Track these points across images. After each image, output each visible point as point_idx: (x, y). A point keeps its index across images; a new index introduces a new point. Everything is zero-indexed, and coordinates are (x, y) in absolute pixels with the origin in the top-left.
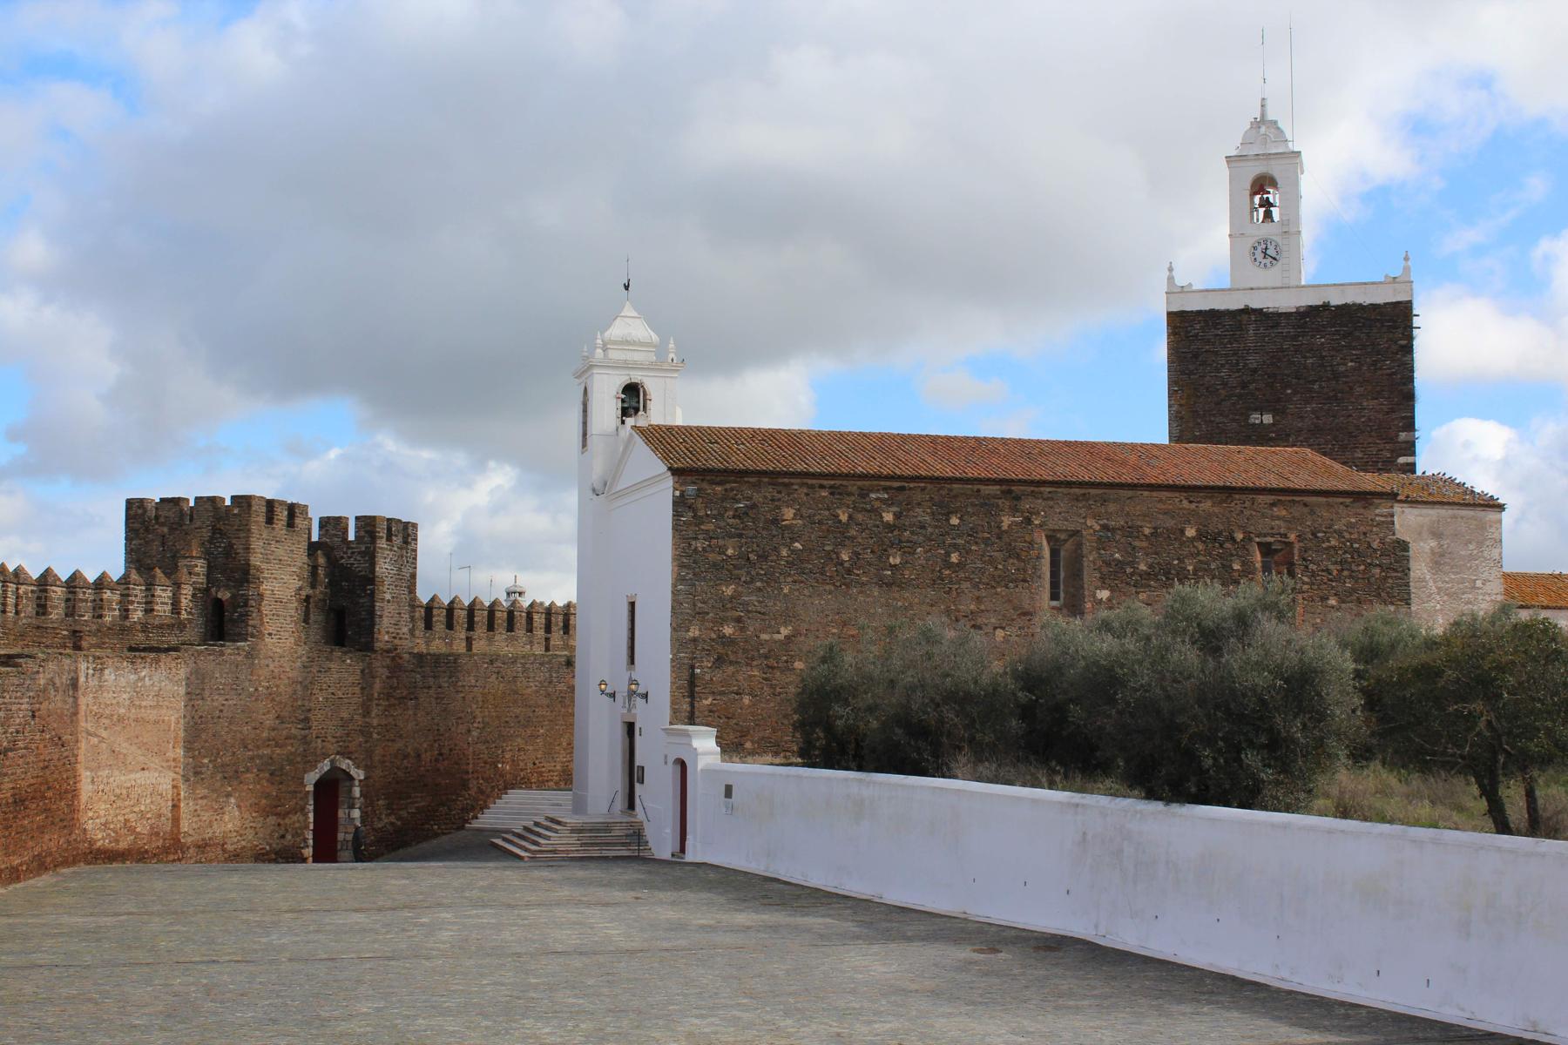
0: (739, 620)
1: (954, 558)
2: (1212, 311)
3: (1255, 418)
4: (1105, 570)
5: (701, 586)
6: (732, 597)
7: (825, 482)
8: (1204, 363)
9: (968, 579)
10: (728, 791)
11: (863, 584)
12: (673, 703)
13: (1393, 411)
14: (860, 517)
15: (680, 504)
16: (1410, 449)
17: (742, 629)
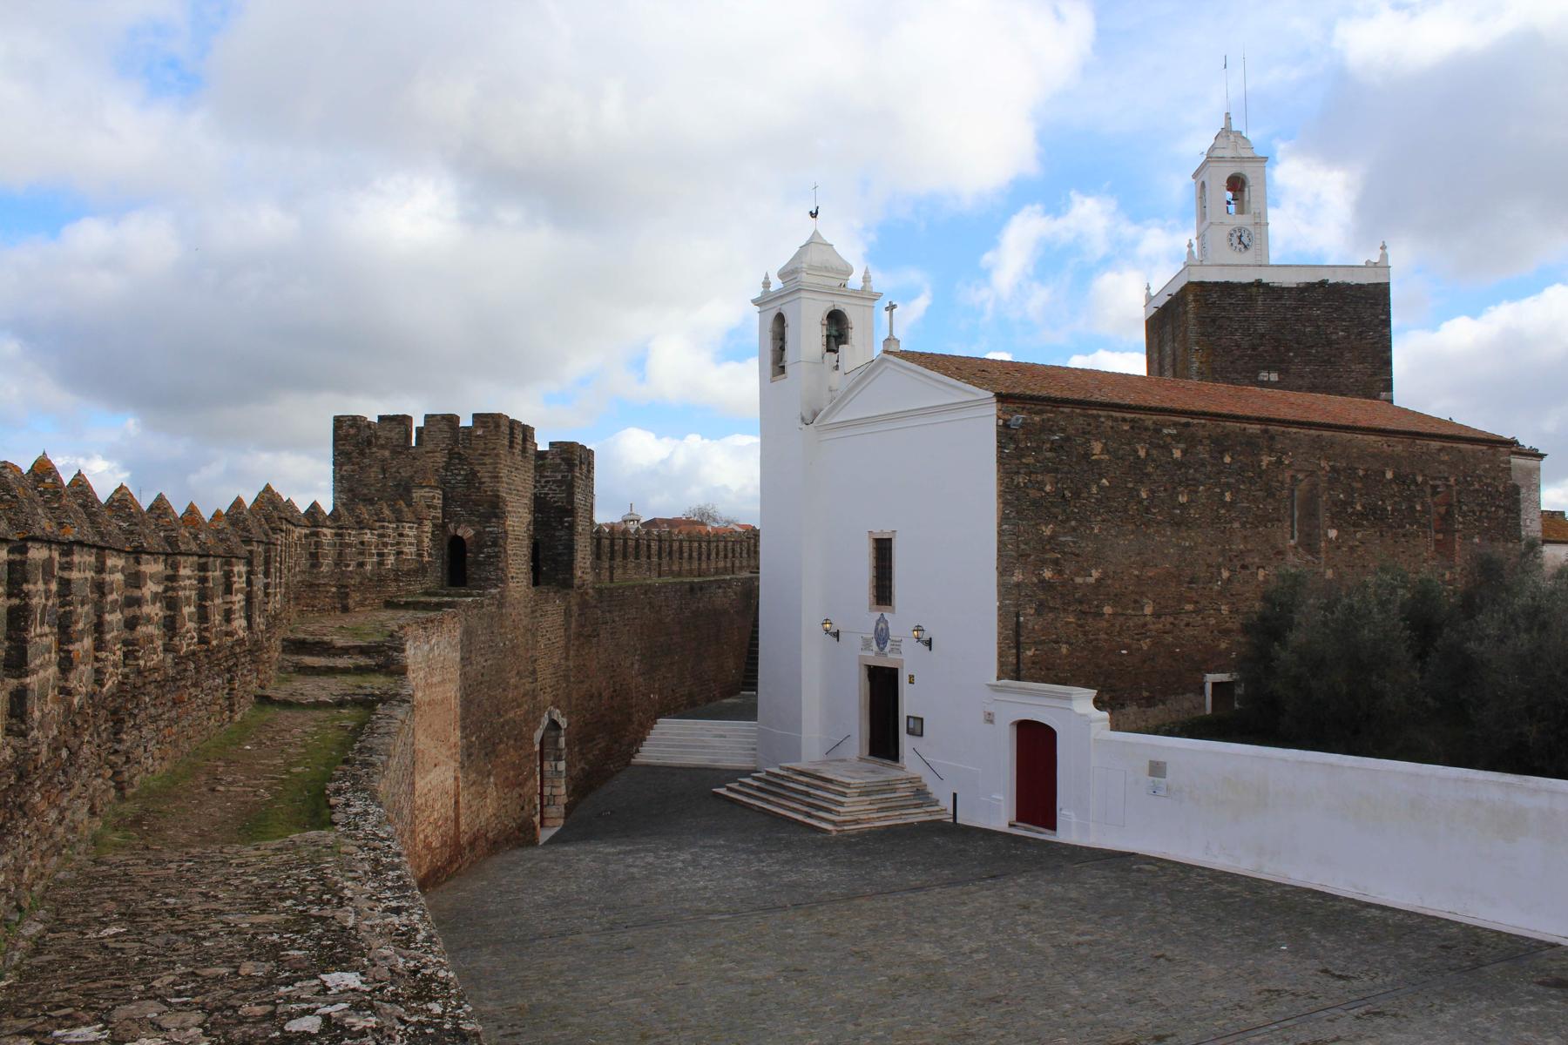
0: (1056, 562)
3: (1264, 376)
4: (1334, 509)
6: (1051, 537)
7: (1128, 416)
8: (1220, 327)
12: (1000, 655)
13: (1375, 374)
15: (1005, 434)
17: (1060, 572)
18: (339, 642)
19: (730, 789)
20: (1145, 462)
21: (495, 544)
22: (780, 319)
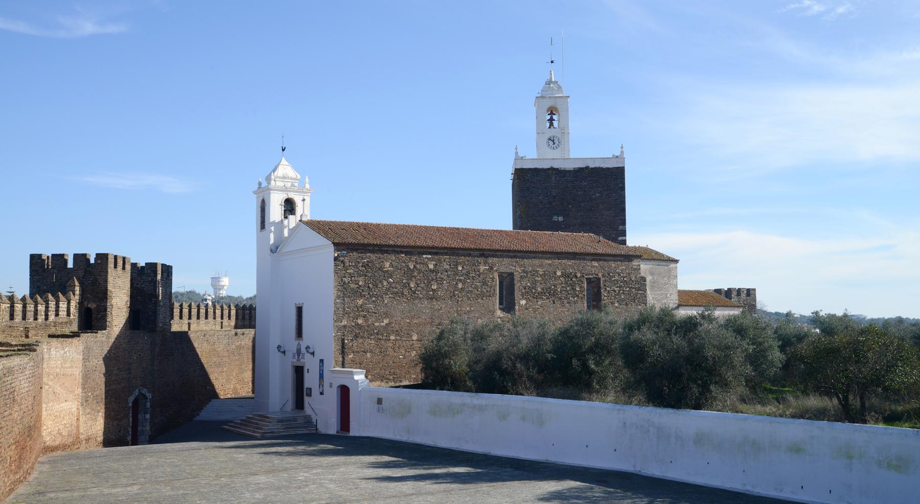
0: (365, 316)
1: (460, 285)
2: (536, 169)
3: (555, 218)
10: (380, 401)
11: (420, 299)
16: (624, 233)
18: (13, 343)
20: (413, 271)
22: (263, 201)
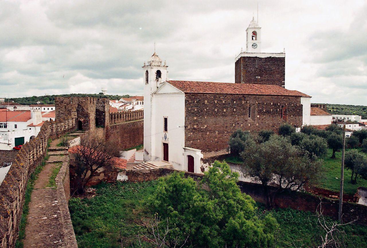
0: (197, 124)
1: (235, 110)
3: (257, 77)
5: (190, 118)
7: (213, 95)
8: (248, 67)
9: (237, 114)
11: (219, 116)
13: (281, 77)
14: (219, 102)
19: (136, 167)
21: (87, 122)
